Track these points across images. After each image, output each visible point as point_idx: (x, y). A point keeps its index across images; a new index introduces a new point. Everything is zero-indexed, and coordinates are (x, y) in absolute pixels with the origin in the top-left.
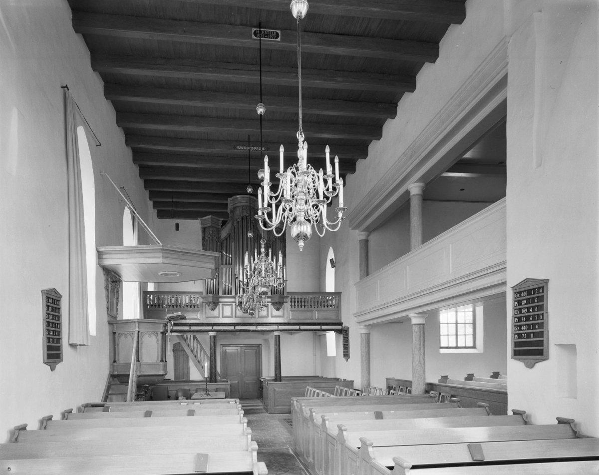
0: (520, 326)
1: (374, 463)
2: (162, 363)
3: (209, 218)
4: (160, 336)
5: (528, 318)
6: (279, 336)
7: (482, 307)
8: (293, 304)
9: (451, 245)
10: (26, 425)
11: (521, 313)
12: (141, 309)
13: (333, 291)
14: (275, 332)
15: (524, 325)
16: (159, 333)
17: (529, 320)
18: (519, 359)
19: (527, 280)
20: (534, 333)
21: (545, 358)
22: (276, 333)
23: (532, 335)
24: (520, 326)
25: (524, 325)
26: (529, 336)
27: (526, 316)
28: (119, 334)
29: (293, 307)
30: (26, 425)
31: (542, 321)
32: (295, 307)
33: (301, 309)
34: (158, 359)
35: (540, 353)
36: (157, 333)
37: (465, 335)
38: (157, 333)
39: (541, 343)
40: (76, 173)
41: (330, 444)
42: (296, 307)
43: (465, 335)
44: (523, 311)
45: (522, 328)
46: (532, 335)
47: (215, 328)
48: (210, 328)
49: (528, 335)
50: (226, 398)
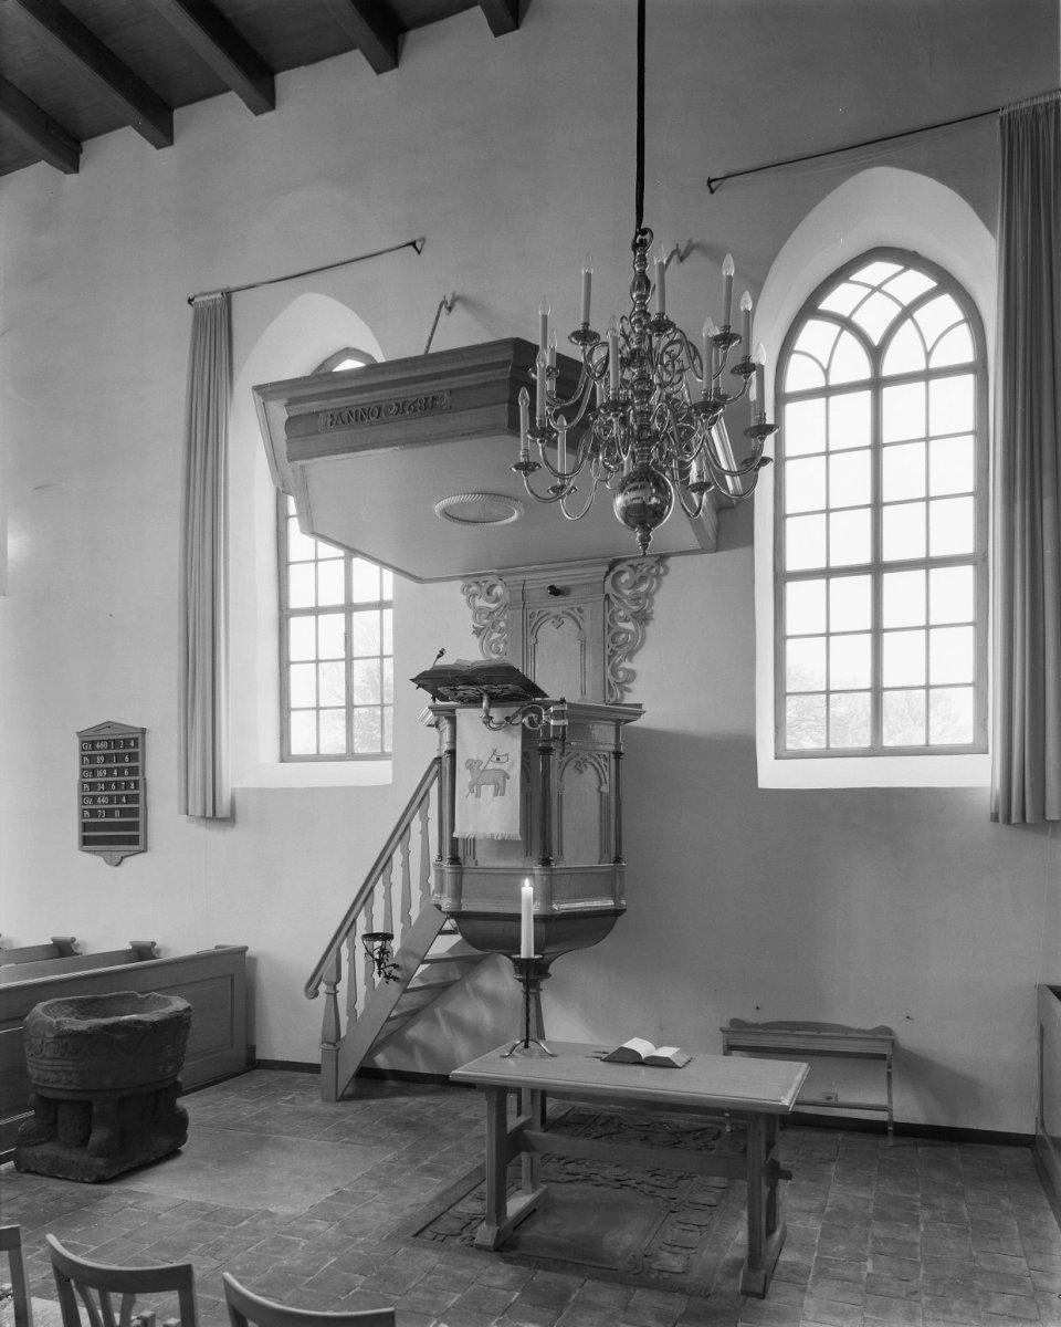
0: (94, 798)
1: (278, 398)
5: (108, 785)
7: (137, 1295)
9: (694, 495)
10: (246, 948)
11: (95, 802)
15: (101, 796)
17: (110, 790)
18: (94, 852)
19: (108, 725)
20: (120, 809)
21: (142, 849)
23: (117, 813)
24: (94, 798)
25: (101, 796)
26: (110, 813)
27: (105, 783)
30: (246, 948)
31: (135, 792)
35: (134, 840)
39: (135, 826)
40: (209, 491)
43: (828, 692)
44: (99, 773)
45: (99, 801)
46: (117, 813)
49: (110, 813)
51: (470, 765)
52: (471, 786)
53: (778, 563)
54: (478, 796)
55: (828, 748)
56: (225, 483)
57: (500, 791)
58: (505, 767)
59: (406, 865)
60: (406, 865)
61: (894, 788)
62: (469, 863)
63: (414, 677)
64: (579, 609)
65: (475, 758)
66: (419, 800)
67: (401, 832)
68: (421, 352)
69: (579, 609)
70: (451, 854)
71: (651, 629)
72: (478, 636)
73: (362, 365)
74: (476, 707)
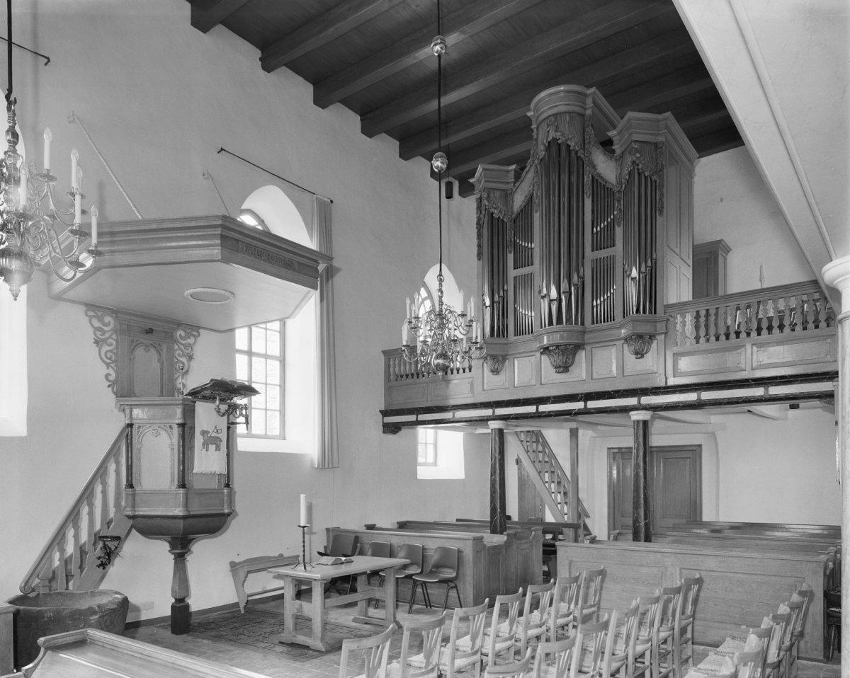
2: (182, 491)
3: (518, 363)
4: (176, 431)
6: (645, 423)
8: (702, 332)
12: (323, 386)
13: (425, 434)
14: (632, 413)
16: (175, 427)
22: (636, 416)
28: (139, 427)
29: (702, 340)
32: (708, 340)
33: (708, 346)
34: (172, 481)
36: (170, 427)
37: (266, 410)
38: (170, 427)
41: (650, 644)
42: (713, 339)
47: (645, 400)
48: (632, 401)
50: (693, 246)
51: (204, 433)
52: (204, 444)
53: (574, 445)
54: (207, 450)
55: (266, 434)
56: (645, 488)
57: (218, 448)
58: (220, 435)
59: (104, 492)
60: (104, 492)
61: (260, 452)
62: (137, 488)
63: (106, 368)
64: (159, 344)
65: (206, 430)
66: (113, 452)
67: (101, 472)
68: (13, 41)
69: (159, 344)
70: (128, 481)
71: (193, 363)
72: (97, 346)
73: (261, 229)
74: (212, 403)
